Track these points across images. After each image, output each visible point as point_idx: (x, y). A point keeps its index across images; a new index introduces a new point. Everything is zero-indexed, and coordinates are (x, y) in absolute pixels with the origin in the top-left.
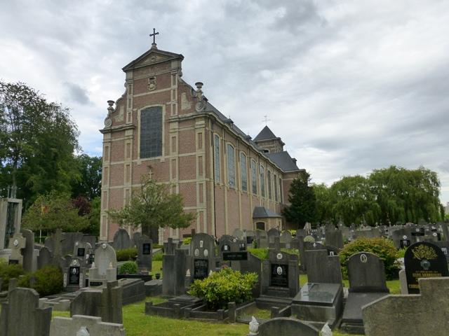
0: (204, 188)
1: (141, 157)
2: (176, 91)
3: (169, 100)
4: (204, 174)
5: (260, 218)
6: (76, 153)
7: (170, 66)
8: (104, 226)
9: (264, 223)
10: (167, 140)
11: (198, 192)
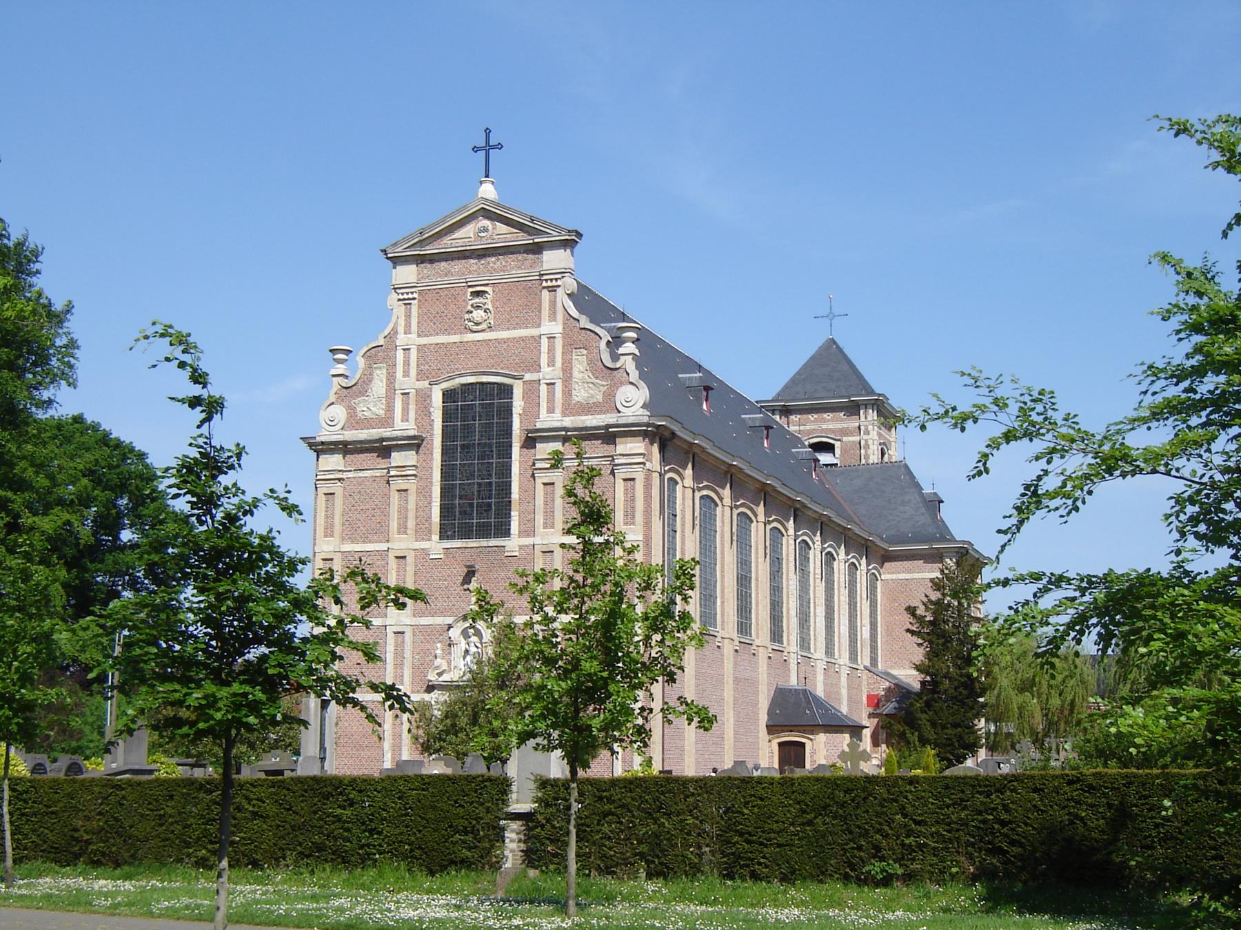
1: (443, 536)
2: (559, 343)
5: (791, 728)
6: (65, 402)
9: (803, 745)
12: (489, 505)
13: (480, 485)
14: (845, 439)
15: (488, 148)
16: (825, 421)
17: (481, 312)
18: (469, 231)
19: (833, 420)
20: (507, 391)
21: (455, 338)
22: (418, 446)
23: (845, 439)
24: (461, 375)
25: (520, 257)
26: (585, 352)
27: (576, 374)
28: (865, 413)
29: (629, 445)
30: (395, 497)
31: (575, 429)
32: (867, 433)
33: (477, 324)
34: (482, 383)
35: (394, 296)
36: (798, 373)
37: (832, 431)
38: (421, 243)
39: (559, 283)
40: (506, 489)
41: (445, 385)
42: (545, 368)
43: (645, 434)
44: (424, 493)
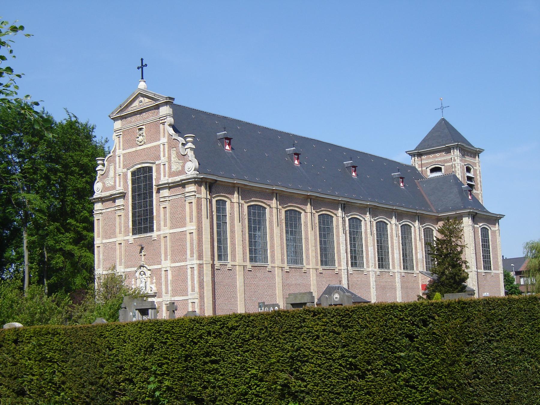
0: (196, 272)
2: (166, 146)
3: (159, 158)
4: (195, 256)
7: (158, 113)
8: (306, 223)
10: (158, 211)
11: (189, 277)
12: (147, 219)
13: (144, 210)
14: (446, 164)
15: (142, 67)
16: (437, 157)
17: (141, 137)
18: (136, 103)
19: (440, 156)
20: (150, 169)
21: (134, 149)
22: (124, 196)
23: (446, 164)
24: (136, 165)
25: (153, 111)
26: (175, 149)
27: (173, 159)
28: (453, 152)
29: (190, 188)
30: (118, 218)
31: (172, 183)
32: (455, 160)
33: (141, 142)
34: (143, 167)
35: (115, 134)
36: (427, 136)
37: (440, 161)
38: (121, 111)
39: (165, 120)
40: (152, 210)
41: (132, 170)
42: (162, 158)
43: (195, 182)
44: (127, 216)
